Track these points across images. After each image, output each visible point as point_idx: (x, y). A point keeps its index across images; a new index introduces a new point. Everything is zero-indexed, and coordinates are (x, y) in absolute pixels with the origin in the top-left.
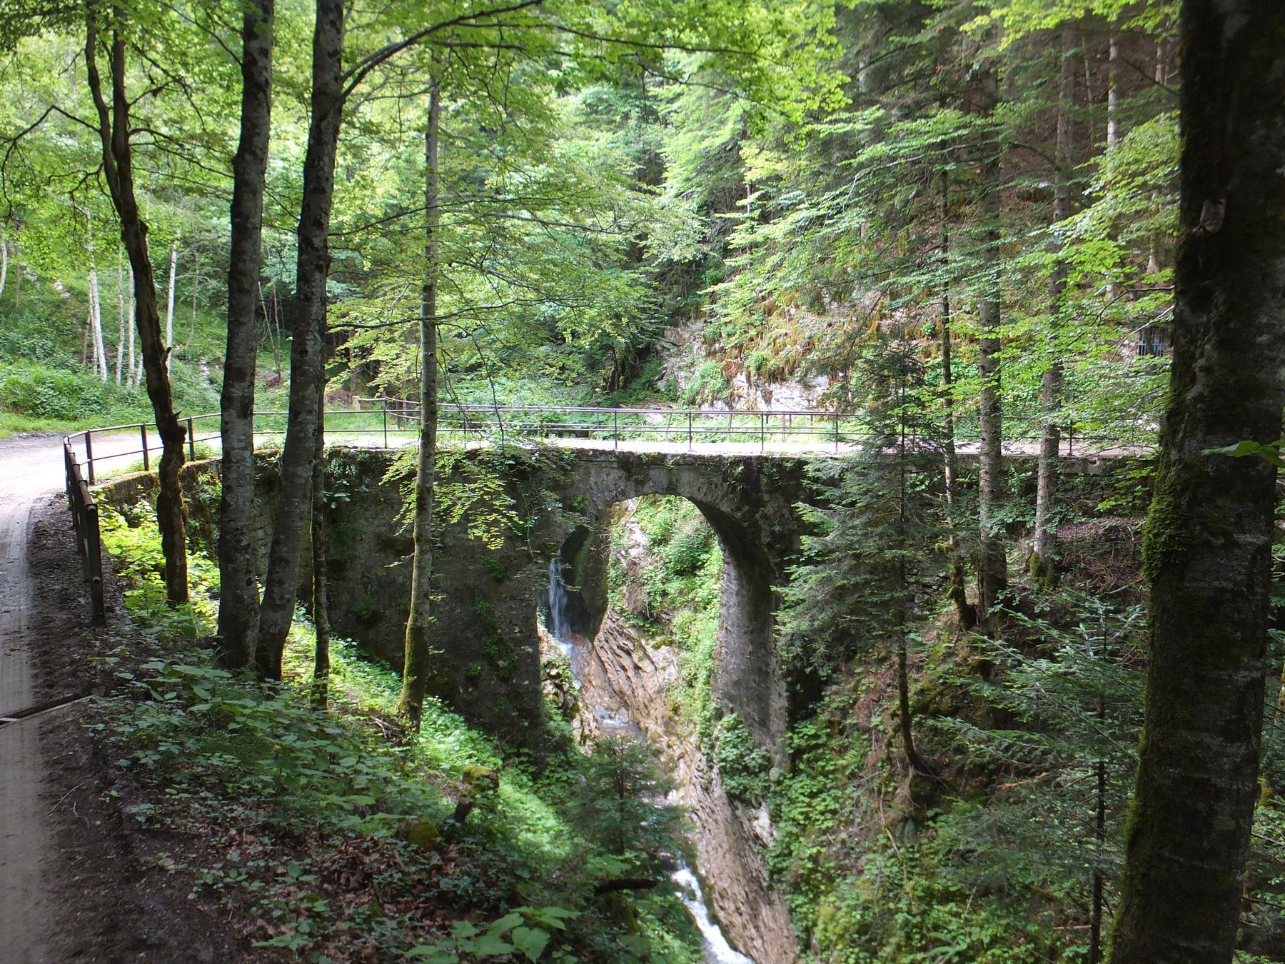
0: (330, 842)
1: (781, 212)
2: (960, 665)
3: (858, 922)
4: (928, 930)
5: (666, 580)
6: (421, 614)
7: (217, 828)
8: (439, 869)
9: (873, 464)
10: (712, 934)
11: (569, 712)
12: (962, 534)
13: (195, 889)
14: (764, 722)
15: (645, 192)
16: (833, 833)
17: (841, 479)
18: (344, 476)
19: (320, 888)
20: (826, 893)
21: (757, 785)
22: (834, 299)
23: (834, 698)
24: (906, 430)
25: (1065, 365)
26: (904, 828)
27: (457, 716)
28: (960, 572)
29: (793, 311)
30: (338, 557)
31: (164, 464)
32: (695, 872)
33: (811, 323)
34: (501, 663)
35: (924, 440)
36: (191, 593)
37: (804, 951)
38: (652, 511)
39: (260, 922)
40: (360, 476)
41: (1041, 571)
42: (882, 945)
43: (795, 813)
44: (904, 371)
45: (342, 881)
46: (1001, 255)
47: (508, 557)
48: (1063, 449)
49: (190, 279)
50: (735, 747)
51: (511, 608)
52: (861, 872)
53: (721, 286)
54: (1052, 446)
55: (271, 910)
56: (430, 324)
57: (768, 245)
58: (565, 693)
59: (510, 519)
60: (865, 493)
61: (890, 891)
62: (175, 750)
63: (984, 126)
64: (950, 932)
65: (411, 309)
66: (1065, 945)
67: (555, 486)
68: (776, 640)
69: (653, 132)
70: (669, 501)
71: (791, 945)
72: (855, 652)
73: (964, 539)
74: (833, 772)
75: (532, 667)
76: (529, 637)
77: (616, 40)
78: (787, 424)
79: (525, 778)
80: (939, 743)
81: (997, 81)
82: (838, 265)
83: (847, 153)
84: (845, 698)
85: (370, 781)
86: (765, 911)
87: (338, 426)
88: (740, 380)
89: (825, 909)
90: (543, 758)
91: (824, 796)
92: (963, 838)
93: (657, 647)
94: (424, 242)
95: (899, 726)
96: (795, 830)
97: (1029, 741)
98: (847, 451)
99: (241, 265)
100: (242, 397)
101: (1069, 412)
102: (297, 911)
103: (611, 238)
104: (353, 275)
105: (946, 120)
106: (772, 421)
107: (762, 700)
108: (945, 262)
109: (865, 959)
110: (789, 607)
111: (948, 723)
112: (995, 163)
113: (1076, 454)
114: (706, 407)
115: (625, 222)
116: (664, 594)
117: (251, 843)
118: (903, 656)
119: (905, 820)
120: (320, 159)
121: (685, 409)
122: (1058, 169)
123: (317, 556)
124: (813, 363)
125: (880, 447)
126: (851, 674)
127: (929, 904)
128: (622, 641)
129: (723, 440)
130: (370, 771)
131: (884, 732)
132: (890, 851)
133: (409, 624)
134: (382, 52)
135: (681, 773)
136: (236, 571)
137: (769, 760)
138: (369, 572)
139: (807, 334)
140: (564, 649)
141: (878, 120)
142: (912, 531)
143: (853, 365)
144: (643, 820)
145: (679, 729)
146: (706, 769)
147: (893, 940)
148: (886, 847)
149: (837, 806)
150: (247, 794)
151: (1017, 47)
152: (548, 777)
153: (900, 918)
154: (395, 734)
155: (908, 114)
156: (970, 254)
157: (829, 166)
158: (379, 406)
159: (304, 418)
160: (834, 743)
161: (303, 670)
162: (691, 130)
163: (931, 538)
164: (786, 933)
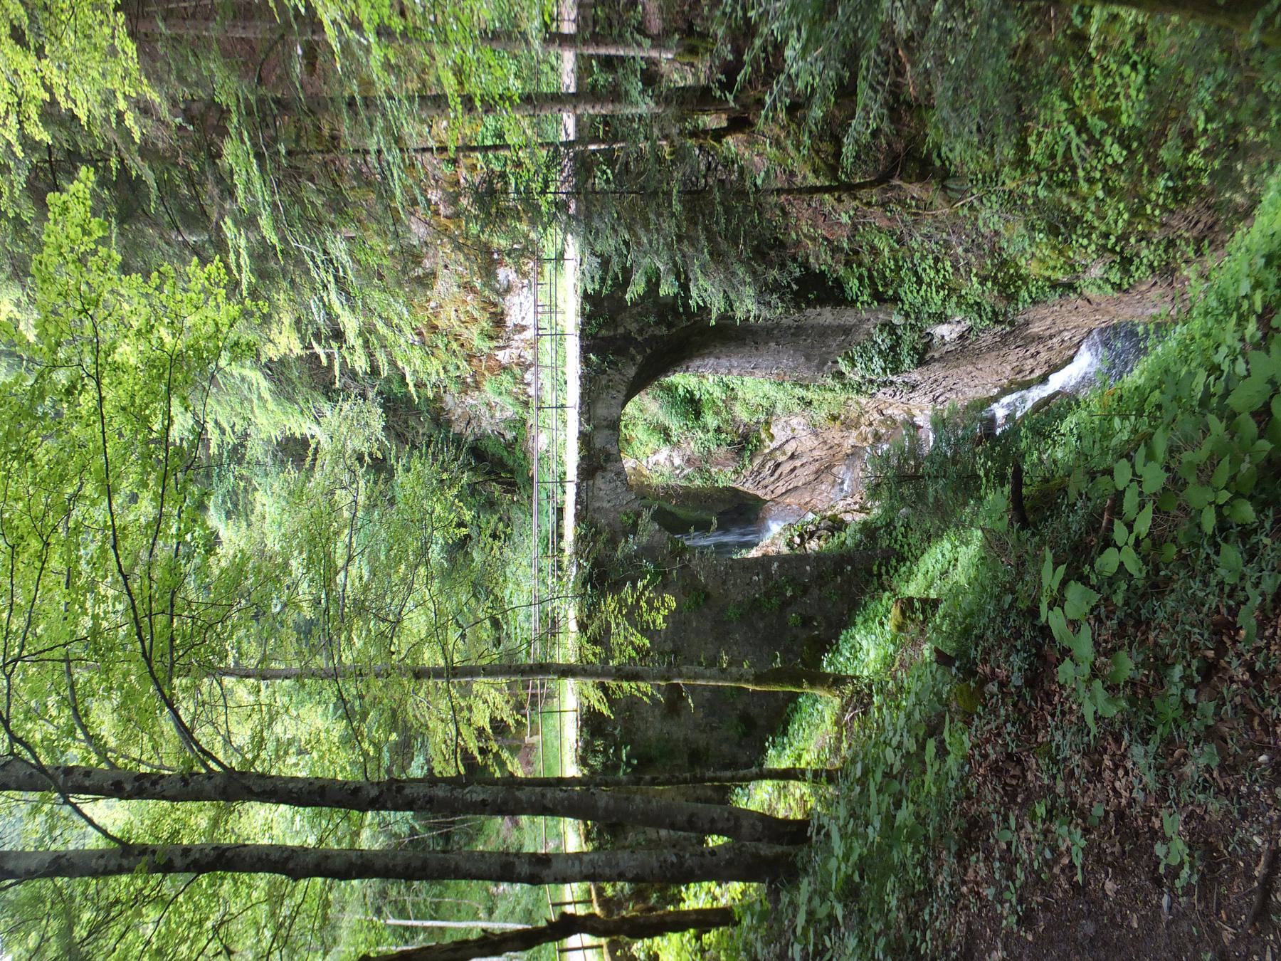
0: (974, 790)
1: (331, 318)
2: (789, 133)
3: (1047, 235)
4: (1055, 164)
5: (705, 429)
6: (742, 675)
7: (960, 905)
8: (1002, 685)
9: (586, 223)
10: (1057, 381)
11: (836, 525)
12: (656, 131)
13: (1022, 933)
14: (847, 331)
15: (315, 460)
16: (957, 261)
17: (601, 255)
18: (605, 752)
19: (1022, 806)
20: (1018, 267)
21: (909, 337)
22: (419, 264)
23: (821, 260)
24: (552, 189)
25: (483, 26)
26: (952, 190)
27: (842, 637)
28: (694, 134)
29: (432, 304)
30: (686, 757)
31: (595, 932)
32: (995, 399)
33: (445, 286)
34: (789, 594)
35: (562, 171)
36: (723, 903)
37: (1075, 290)
38: (635, 444)
39: (1056, 870)
40: (604, 736)
41: (693, 51)
42: (1069, 211)
43: (938, 299)
44: (492, 192)
45: (1014, 782)
46: (371, 94)
47: (684, 588)
48: (568, 28)
49: (413, 905)
50: (871, 359)
51: (735, 584)
52: (997, 233)
53: (409, 379)
54: (565, 40)
55: (1044, 858)
56: (452, 672)
57: (367, 332)
58: (818, 529)
59: (645, 588)
60: (615, 231)
61: (1015, 203)
62: (882, 941)
63: (240, 113)
64: (1057, 143)
65: (438, 690)
66: (1071, 25)
67: (613, 542)
68: (765, 319)
69: (255, 450)
70: (626, 427)
71: (1069, 302)
72: (776, 239)
73: (661, 130)
74: (896, 261)
75: (792, 563)
76: (763, 566)
77: (161, 499)
78: (547, 309)
79: (903, 569)
80: (867, 154)
81: (193, 100)
82: (385, 262)
83: (271, 254)
84: (822, 249)
85: (909, 732)
86: (1035, 329)
87: (555, 757)
88: (503, 356)
89: (1034, 269)
90: (883, 550)
91: (920, 270)
92: (966, 136)
93: (772, 437)
94: (371, 678)
95: (850, 195)
96: (954, 299)
97: (868, 69)
98: (573, 249)
99: (399, 869)
100: (530, 863)
101: (532, 26)
102: (1046, 833)
103: (362, 491)
104: (404, 750)
105: (235, 153)
106: (544, 324)
107: (824, 332)
108: (379, 152)
109: (1083, 229)
110: (731, 306)
111: (848, 150)
112: (277, 102)
113: (573, 17)
114: (531, 391)
115: (346, 478)
116: (718, 430)
117: (975, 871)
118: (779, 191)
119: (945, 188)
120: (291, 791)
121: (533, 411)
122: (282, 37)
123: (685, 781)
124: (484, 285)
125: (569, 216)
126: (798, 243)
127: (1029, 164)
128: (766, 472)
129: (564, 373)
130: (899, 733)
131: (856, 210)
132: (976, 203)
133: (751, 687)
134: (180, 732)
135: (897, 412)
136: (701, 866)
137: (884, 325)
138: (700, 725)
139: (456, 289)
140: (775, 528)
141: (236, 223)
142: (653, 184)
143: (485, 244)
144: (945, 456)
145: (853, 415)
146: (893, 388)
147: (1065, 200)
148: (971, 208)
149: (930, 256)
150: (926, 871)
151: (156, 78)
152: (902, 546)
153: (1042, 193)
154: (861, 700)
155: (230, 192)
156: (371, 124)
157: (284, 272)
158: (535, 717)
159: (548, 797)
160: (867, 260)
161: (798, 792)
162: (252, 411)
163: (660, 163)
164: (1057, 308)
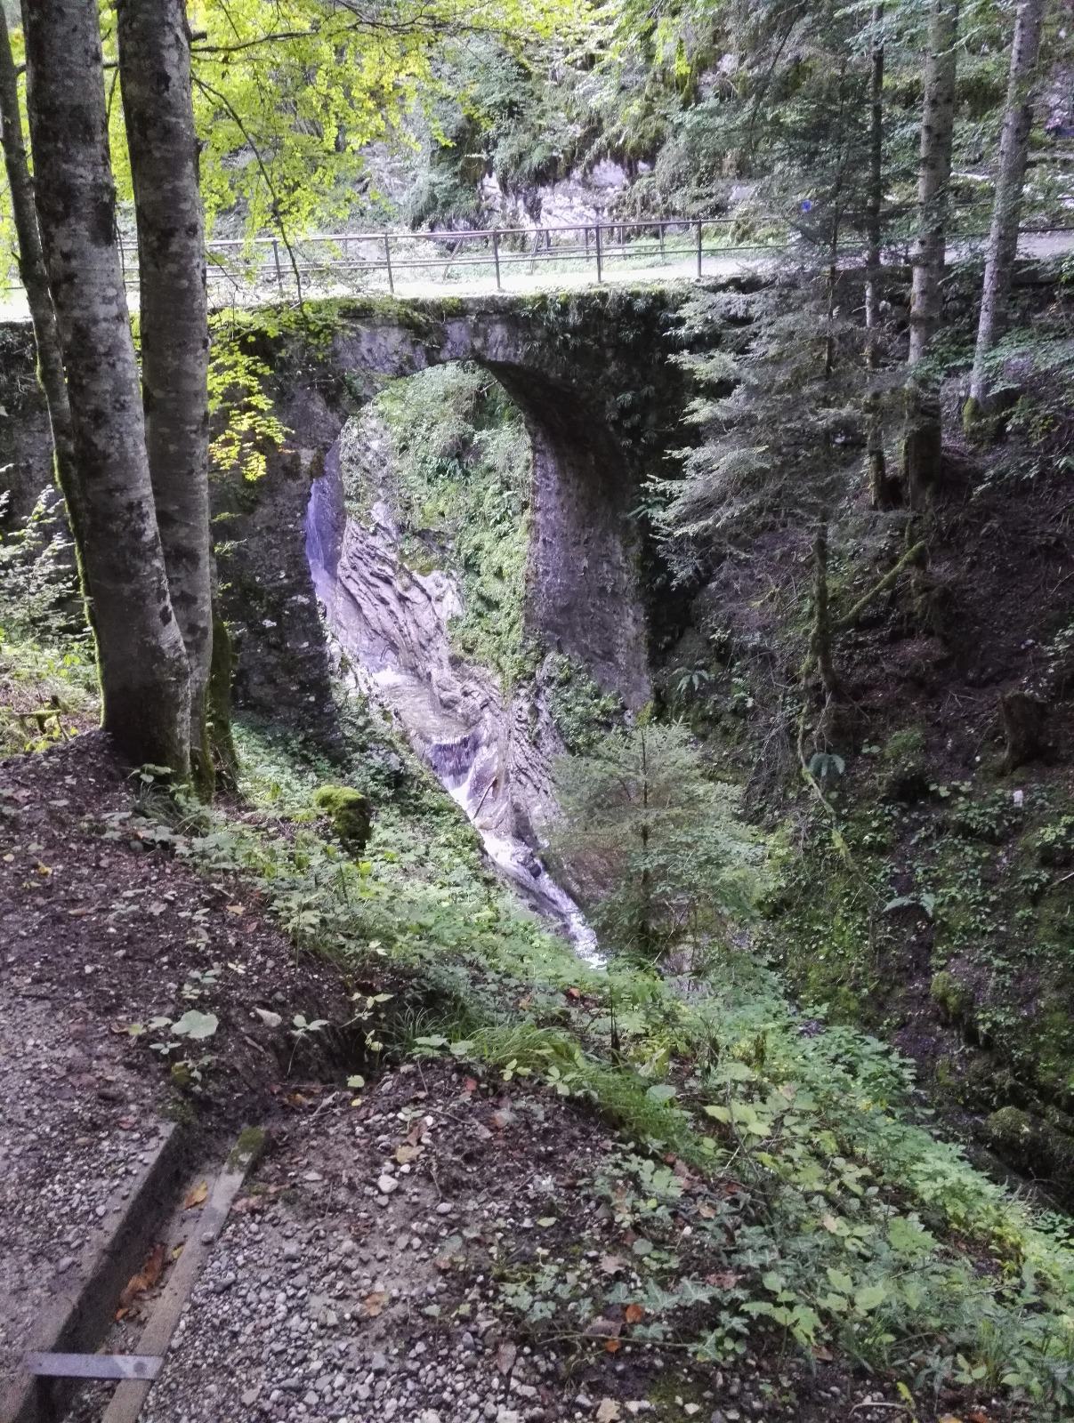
128: (376, 566)
